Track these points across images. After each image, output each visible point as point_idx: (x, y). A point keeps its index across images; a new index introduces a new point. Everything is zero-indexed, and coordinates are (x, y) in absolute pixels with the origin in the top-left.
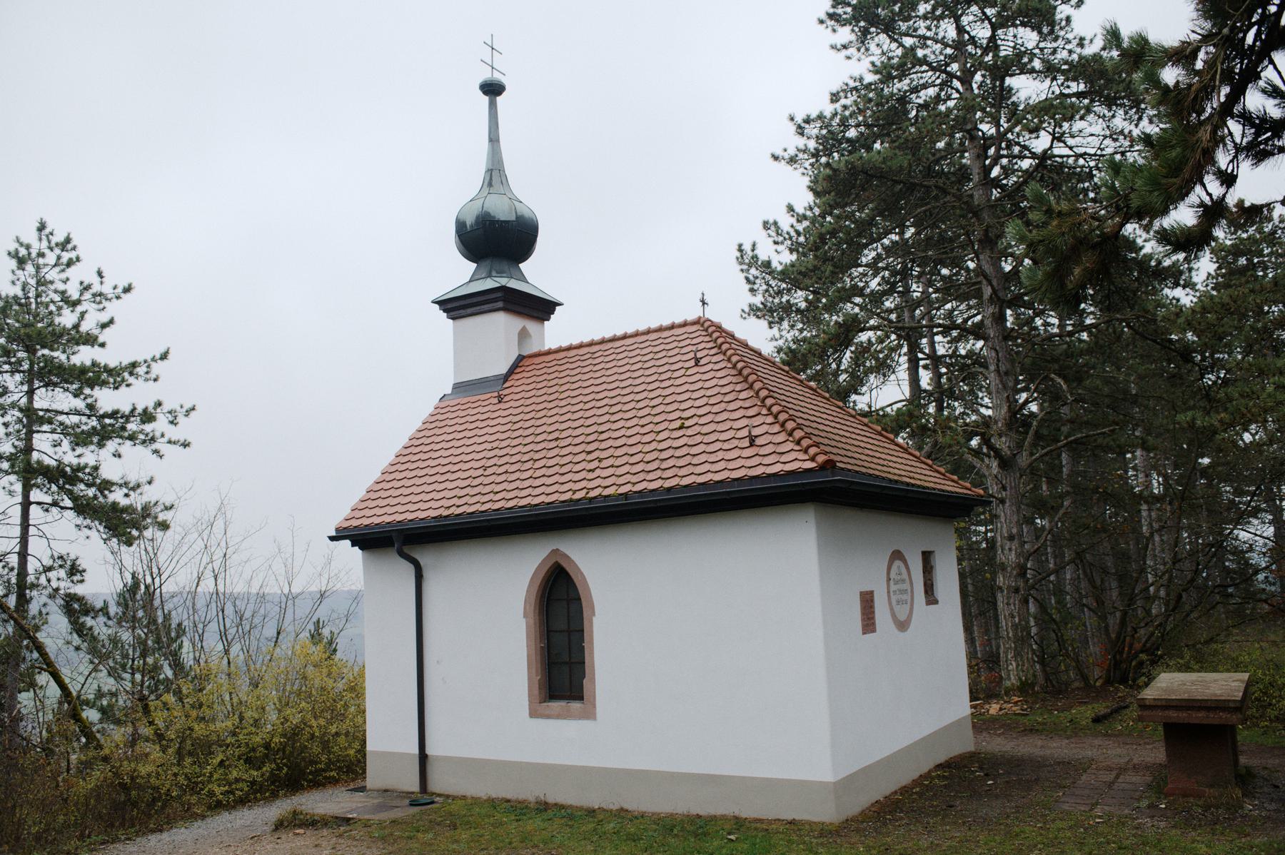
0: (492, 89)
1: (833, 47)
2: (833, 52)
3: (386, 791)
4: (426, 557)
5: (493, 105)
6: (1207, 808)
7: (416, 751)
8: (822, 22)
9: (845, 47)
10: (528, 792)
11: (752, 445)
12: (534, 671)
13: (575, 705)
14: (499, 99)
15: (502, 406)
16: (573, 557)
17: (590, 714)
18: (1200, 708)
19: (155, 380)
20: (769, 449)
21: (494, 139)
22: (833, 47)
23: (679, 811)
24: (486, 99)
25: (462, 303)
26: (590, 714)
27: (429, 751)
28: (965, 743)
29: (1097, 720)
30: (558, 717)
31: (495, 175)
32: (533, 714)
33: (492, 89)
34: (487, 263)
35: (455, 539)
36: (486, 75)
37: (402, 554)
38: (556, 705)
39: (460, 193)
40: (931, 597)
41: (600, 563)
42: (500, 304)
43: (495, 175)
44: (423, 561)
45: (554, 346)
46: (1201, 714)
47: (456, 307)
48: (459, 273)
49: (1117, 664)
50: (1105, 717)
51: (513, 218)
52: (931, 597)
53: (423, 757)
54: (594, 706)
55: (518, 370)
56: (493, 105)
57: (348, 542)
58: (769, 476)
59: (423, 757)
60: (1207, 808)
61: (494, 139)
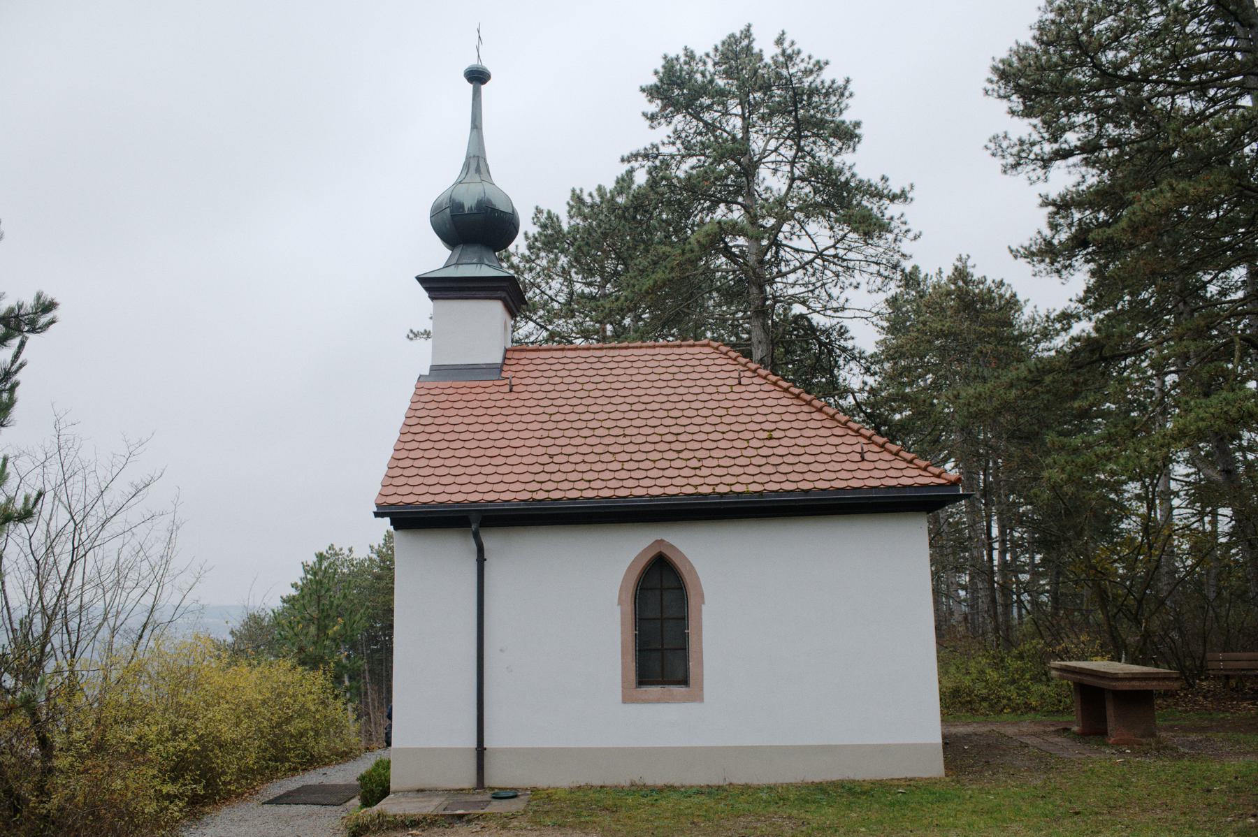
0: (477, 77)
3: (420, 791)
4: (491, 541)
5: (477, 95)
7: (474, 744)
10: (621, 777)
13: (677, 690)
14: (483, 87)
15: (513, 396)
17: (698, 698)
19: (856, 287)
21: (476, 124)
23: (859, 777)
24: (470, 86)
25: (448, 285)
26: (698, 698)
30: (658, 701)
31: (476, 163)
32: (627, 699)
33: (477, 77)
34: (458, 251)
35: (612, 522)
36: (471, 62)
38: (655, 690)
39: (440, 178)
41: (703, 553)
42: (504, 294)
43: (476, 163)
44: (487, 544)
47: (437, 287)
48: (436, 256)
53: (481, 750)
54: (702, 689)
56: (477, 95)
58: (905, 486)
59: (481, 750)
61: (476, 124)
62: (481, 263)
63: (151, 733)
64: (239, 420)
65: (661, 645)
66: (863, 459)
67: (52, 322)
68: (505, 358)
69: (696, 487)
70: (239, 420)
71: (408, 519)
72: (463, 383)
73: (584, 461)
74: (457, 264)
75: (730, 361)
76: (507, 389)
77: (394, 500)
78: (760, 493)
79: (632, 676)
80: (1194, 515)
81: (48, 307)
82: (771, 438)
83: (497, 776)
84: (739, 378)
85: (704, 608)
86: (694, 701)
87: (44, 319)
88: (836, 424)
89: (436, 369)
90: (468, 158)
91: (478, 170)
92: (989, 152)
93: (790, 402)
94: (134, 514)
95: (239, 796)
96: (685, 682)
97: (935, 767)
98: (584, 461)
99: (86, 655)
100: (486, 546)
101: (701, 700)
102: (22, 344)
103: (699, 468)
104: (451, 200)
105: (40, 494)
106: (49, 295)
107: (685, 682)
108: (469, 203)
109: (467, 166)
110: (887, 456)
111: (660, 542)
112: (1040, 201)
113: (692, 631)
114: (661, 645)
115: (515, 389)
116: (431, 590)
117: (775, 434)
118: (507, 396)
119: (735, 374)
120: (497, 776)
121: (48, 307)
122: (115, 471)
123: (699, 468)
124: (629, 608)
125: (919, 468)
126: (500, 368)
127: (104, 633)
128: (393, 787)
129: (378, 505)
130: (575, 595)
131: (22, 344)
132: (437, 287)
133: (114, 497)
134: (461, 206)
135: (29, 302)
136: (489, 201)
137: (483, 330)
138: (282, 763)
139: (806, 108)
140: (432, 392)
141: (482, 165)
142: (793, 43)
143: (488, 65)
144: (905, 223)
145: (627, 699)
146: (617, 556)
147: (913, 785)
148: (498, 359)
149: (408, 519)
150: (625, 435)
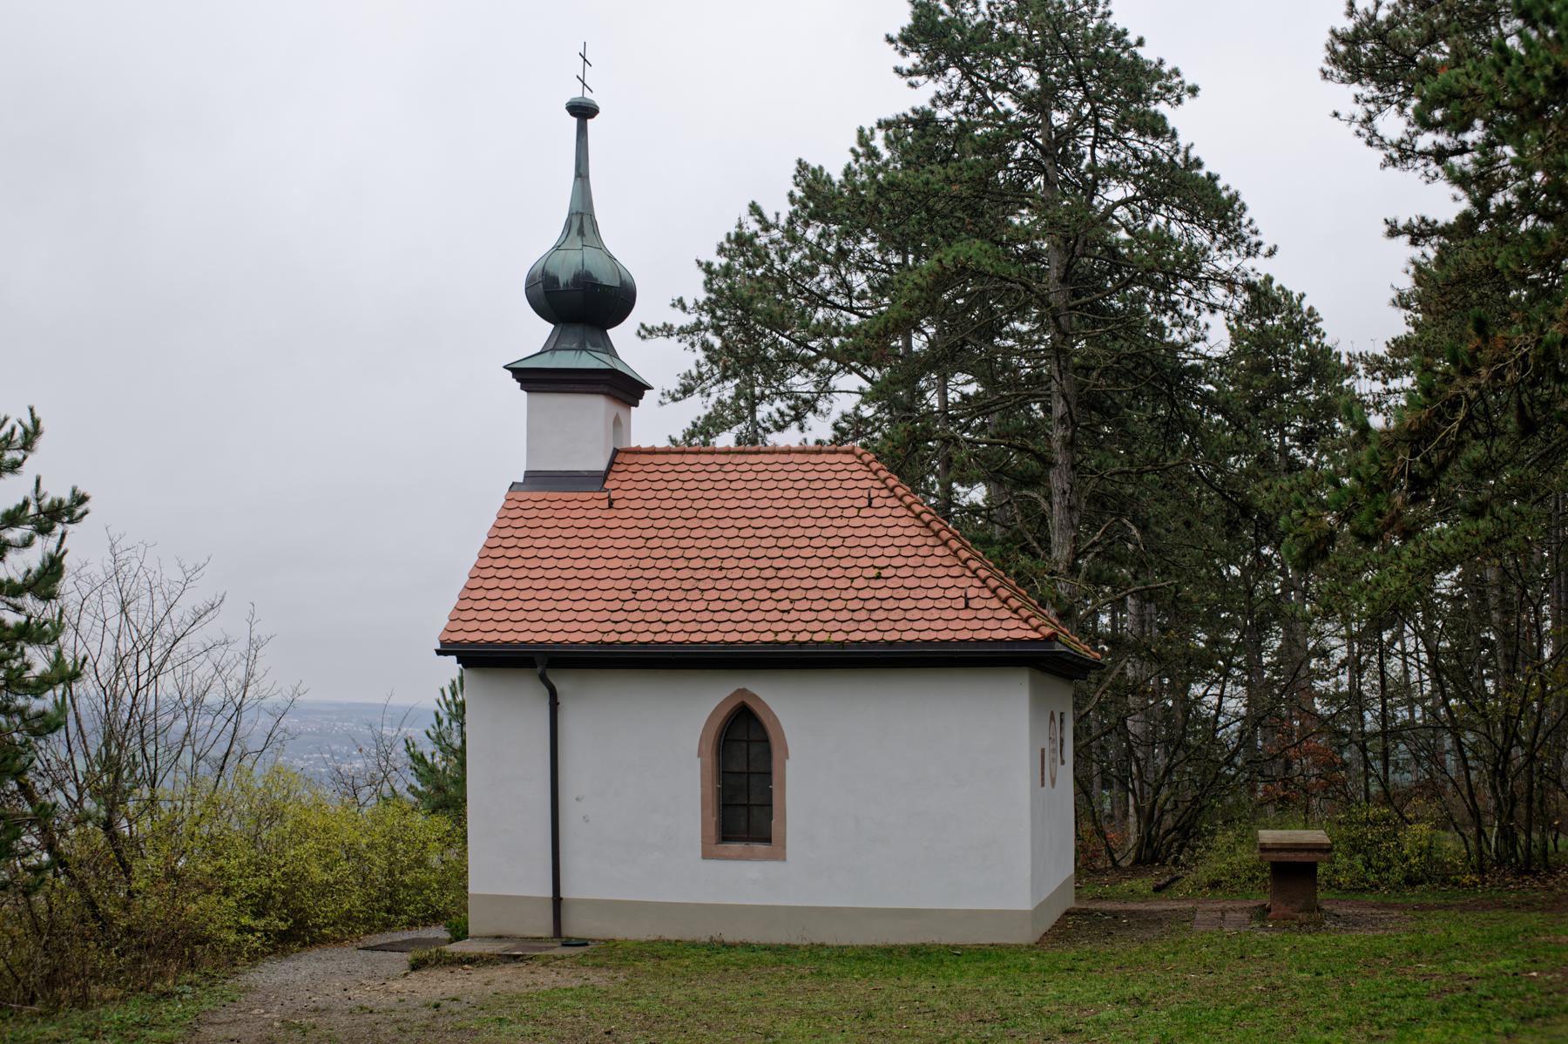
0: (583, 111)
1: (898, 71)
2: (896, 76)
4: (565, 684)
5: (582, 132)
6: (1301, 925)
7: (549, 893)
8: (890, 40)
9: (910, 73)
11: (610, 506)
12: (710, 811)
13: (760, 848)
15: (613, 513)
16: (764, 698)
17: (780, 856)
18: (1309, 850)
20: (627, 513)
21: (582, 172)
22: (898, 71)
26: (780, 856)
27: (565, 893)
28: (1070, 903)
29: (1158, 889)
30: (739, 858)
31: (582, 221)
33: (583, 111)
36: (575, 92)
37: (544, 679)
38: (737, 847)
39: (537, 237)
40: (1063, 763)
41: (789, 706)
43: (582, 221)
45: (645, 445)
46: (1304, 854)
47: (531, 378)
48: (532, 334)
49: (1149, 844)
50: (1164, 887)
51: (617, 284)
52: (1063, 763)
53: (557, 900)
55: (615, 468)
56: (582, 132)
57: (454, 658)
59: (557, 900)
60: (1301, 925)
61: (582, 172)
62: (582, 348)
63: (232, 866)
65: (743, 802)
66: (967, 606)
67: (86, 513)
68: (612, 463)
69: (776, 633)
70: (299, 544)
71: (477, 658)
73: (668, 599)
74: (554, 349)
75: (870, 475)
76: (605, 504)
78: (842, 644)
79: (713, 831)
81: (82, 499)
82: (878, 577)
83: (573, 928)
84: (870, 500)
85: (788, 763)
86: (776, 859)
87: (79, 511)
88: (956, 561)
89: (535, 479)
90: (571, 215)
91: (581, 232)
92: (1363, 140)
94: (196, 639)
95: (336, 941)
98: (668, 599)
99: (167, 784)
100: (558, 689)
101: (704, 857)
102: (63, 536)
103: (788, 611)
104: (544, 273)
105: (85, 659)
106: (82, 490)
108: (564, 277)
109: (569, 224)
110: (995, 603)
112: (1386, 228)
113: (775, 787)
114: (743, 802)
115: (616, 504)
116: (506, 728)
117: (885, 573)
118: (606, 514)
120: (573, 928)
121: (82, 499)
122: (174, 597)
123: (788, 611)
124: (710, 759)
126: (605, 476)
127: (187, 759)
128: (471, 933)
129: (442, 643)
130: (651, 748)
131: (63, 536)
132: (531, 378)
133: (181, 612)
134: (555, 280)
135: (66, 497)
136: (588, 275)
138: (397, 914)
140: (522, 505)
142: (680, 304)
144: (1256, 232)
146: (695, 708)
148: (601, 465)
149: (477, 658)
150: (721, 568)
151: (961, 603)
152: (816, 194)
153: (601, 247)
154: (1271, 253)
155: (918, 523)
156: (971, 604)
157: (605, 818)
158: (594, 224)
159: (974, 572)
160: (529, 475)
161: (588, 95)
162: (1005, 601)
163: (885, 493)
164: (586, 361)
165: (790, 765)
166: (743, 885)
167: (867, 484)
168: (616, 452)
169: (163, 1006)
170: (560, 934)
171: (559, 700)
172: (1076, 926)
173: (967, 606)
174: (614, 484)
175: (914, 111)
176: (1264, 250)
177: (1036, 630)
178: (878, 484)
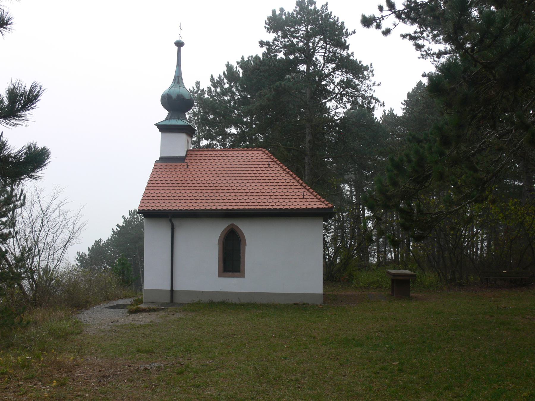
0: (179, 44)
4: (176, 222)
11: (187, 167)
15: (188, 169)
20: (192, 169)
26: (243, 276)
31: (178, 79)
32: (220, 276)
33: (179, 44)
36: (177, 39)
37: (171, 221)
39: (165, 84)
43: (178, 79)
48: (162, 114)
64: (92, 184)
65: (231, 259)
66: (303, 198)
68: (187, 154)
72: (171, 164)
74: (170, 119)
75: (268, 158)
77: (144, 208)
79: (222, 269)
80: (54, 241)
83: (178, 299)
84: (269, 165)
85: (246, 247)
89: (163, 159)
91: (178, 83)
93: (285, 175)
96: (239, 271)
97: (322, 300)
107: (239, 271)
108: (174, 96)
109: (174, 80)
111: (232, 224)
114: (231, 259)
115: (189, 167)
119: (268, 163)
125: (321, 202)
128: (144, 301)
137: (180, 145)
139: (333, 32)
141: (180, 80)
143: (182, 40)
145: (220, 276)
147: (314, 306)
151: (302, 197)
152: (231, 74)
153: (184, 87)
154: (379, 85)
155: (285, 172)
156: (305, 197)
157: (187, 264)
158: (182, 80)
159: (305, 187)
160: (161, 158)
161: (181, 40)
162: (315, 196)
163: (273, 163)
164: (180, 123)
165: (247, 248)
166: (231, 285)
167: (267, 160)
168: (188, 151)
169: (78, 336)
170: (172, 299)
171: (175, 227)
172: (326, 296)
173: (303, 198)
174: (188, 161)
175: (343, 23)
176: (376, 84)
177: (327, 205)
178: (271, 160)
